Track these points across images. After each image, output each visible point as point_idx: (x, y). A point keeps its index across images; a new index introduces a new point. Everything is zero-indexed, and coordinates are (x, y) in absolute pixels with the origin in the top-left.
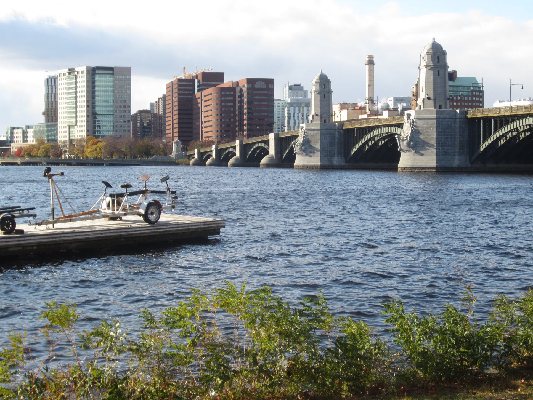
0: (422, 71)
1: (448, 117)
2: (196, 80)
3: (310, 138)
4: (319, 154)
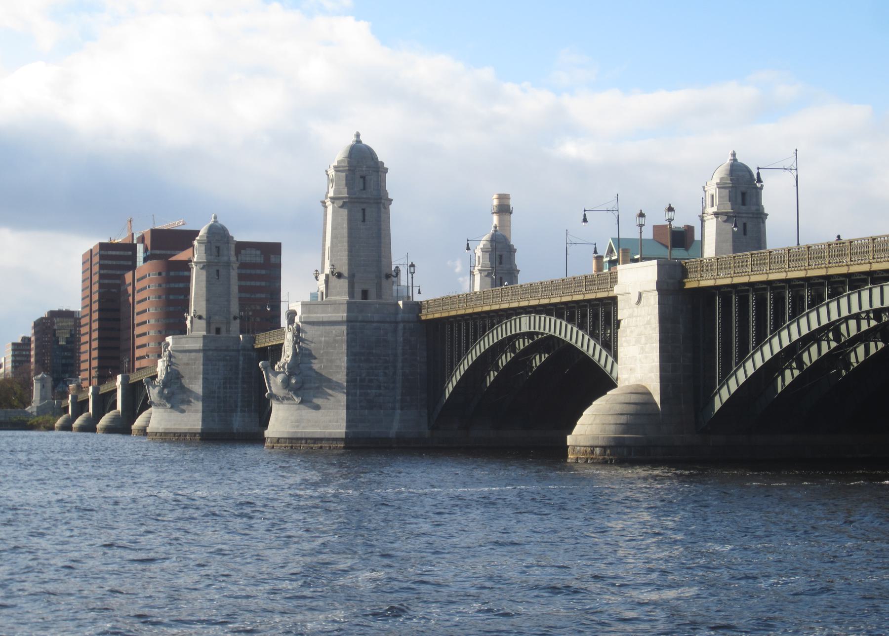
0: (707, 224)
1: (376, 317)
2: (140, 248)
3: (181, 369)
4: (199, 405)
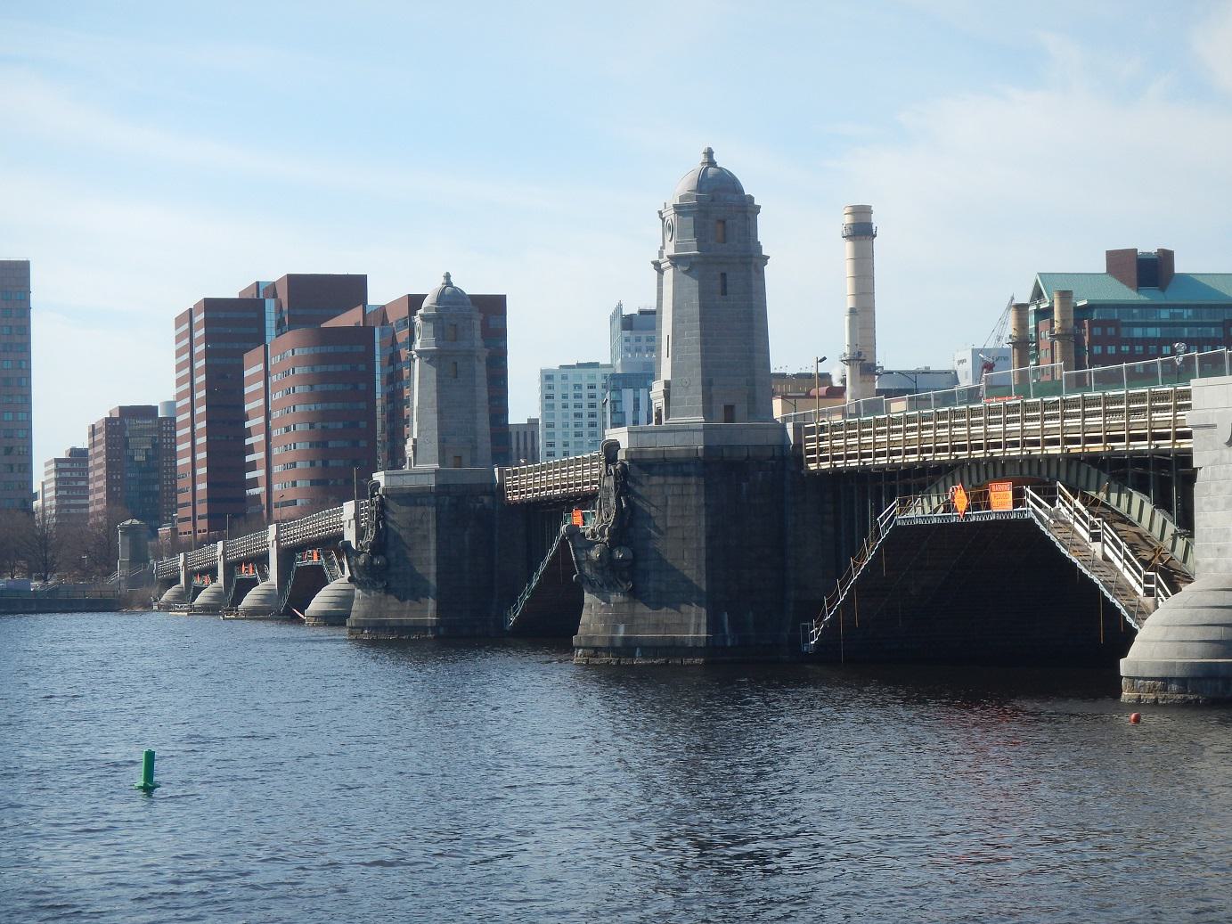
2: (270, 305)
